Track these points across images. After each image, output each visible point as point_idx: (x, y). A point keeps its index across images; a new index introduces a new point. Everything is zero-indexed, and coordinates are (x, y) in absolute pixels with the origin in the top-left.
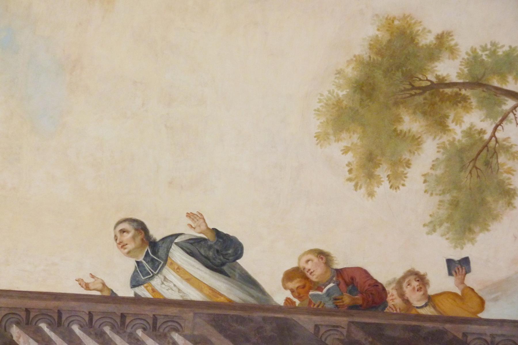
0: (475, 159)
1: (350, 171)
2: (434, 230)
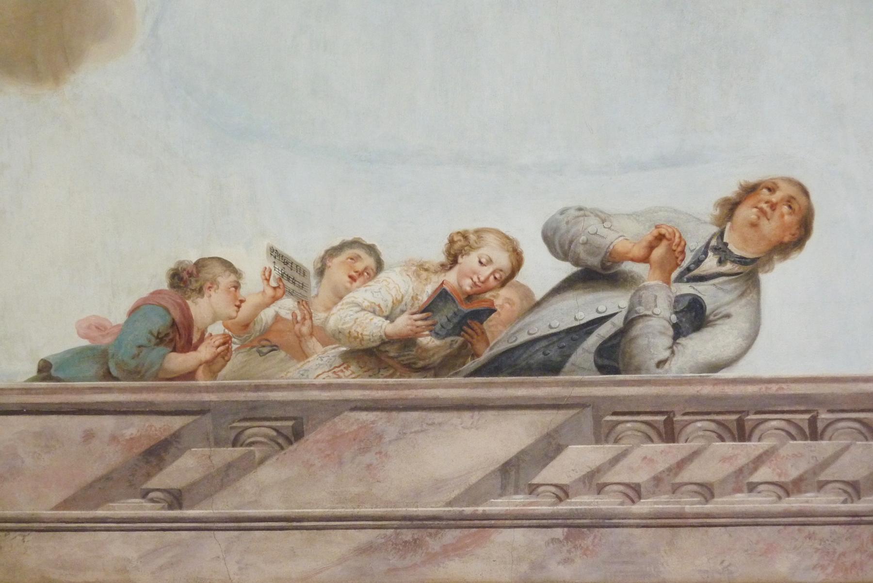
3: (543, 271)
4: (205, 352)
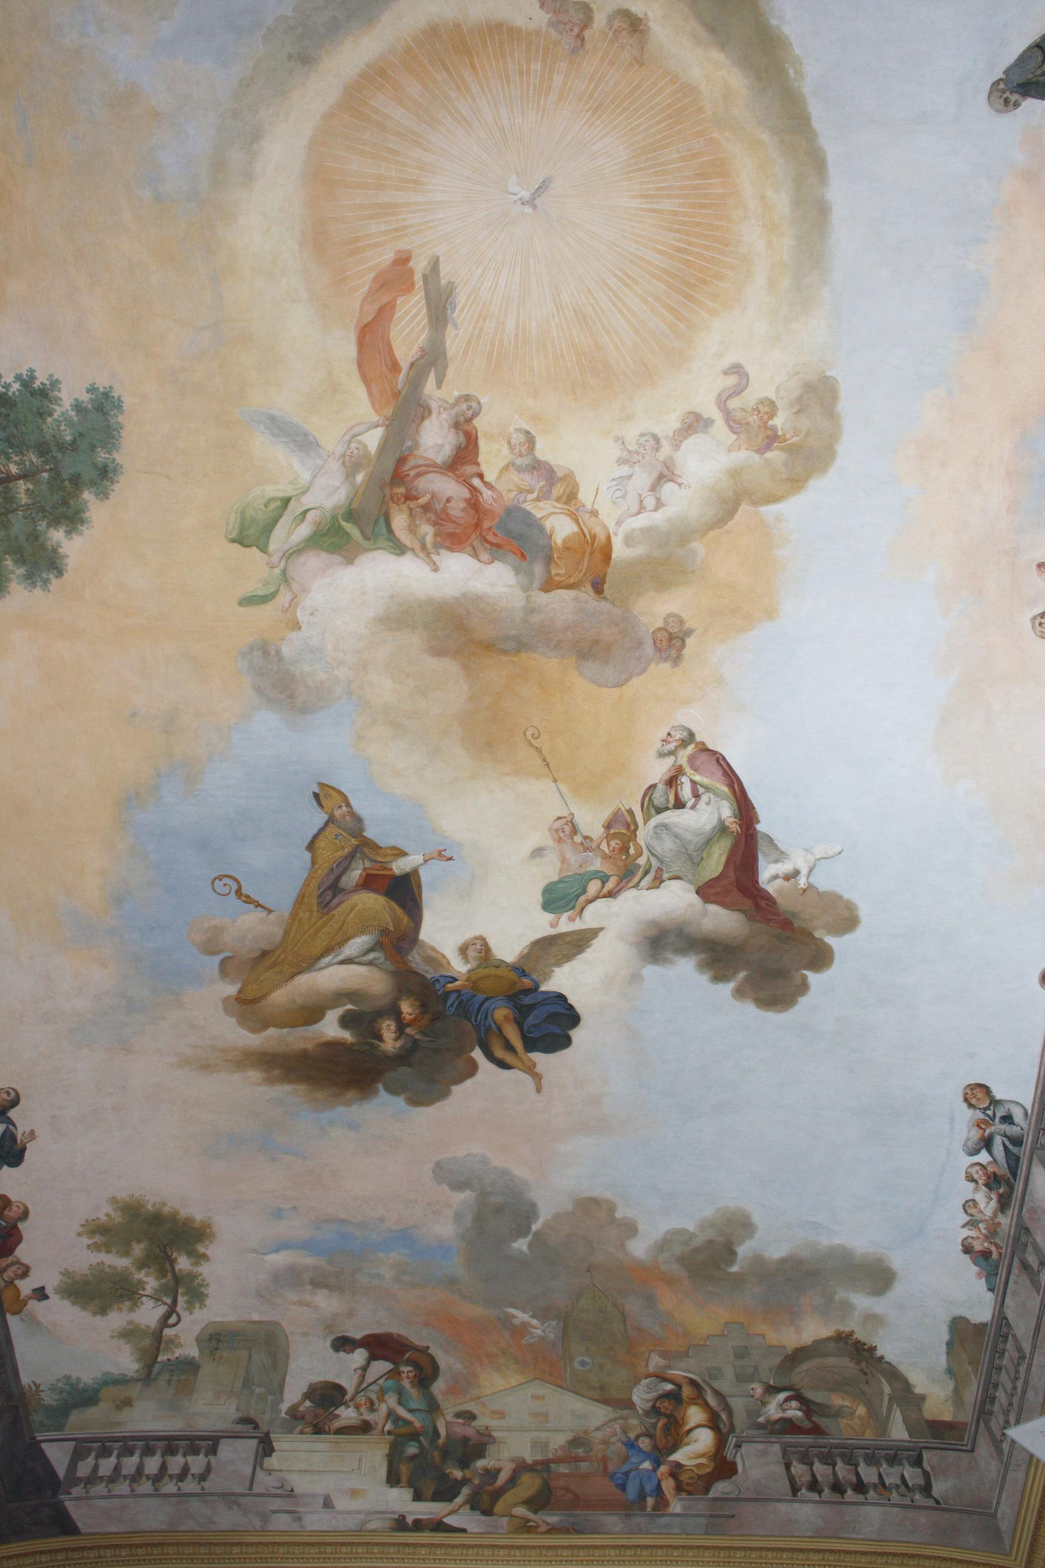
0: (123, 1289)
1: (93, 1220)
2: (64, 1275)
3: (984, 1157)
4: (993, 1249)
